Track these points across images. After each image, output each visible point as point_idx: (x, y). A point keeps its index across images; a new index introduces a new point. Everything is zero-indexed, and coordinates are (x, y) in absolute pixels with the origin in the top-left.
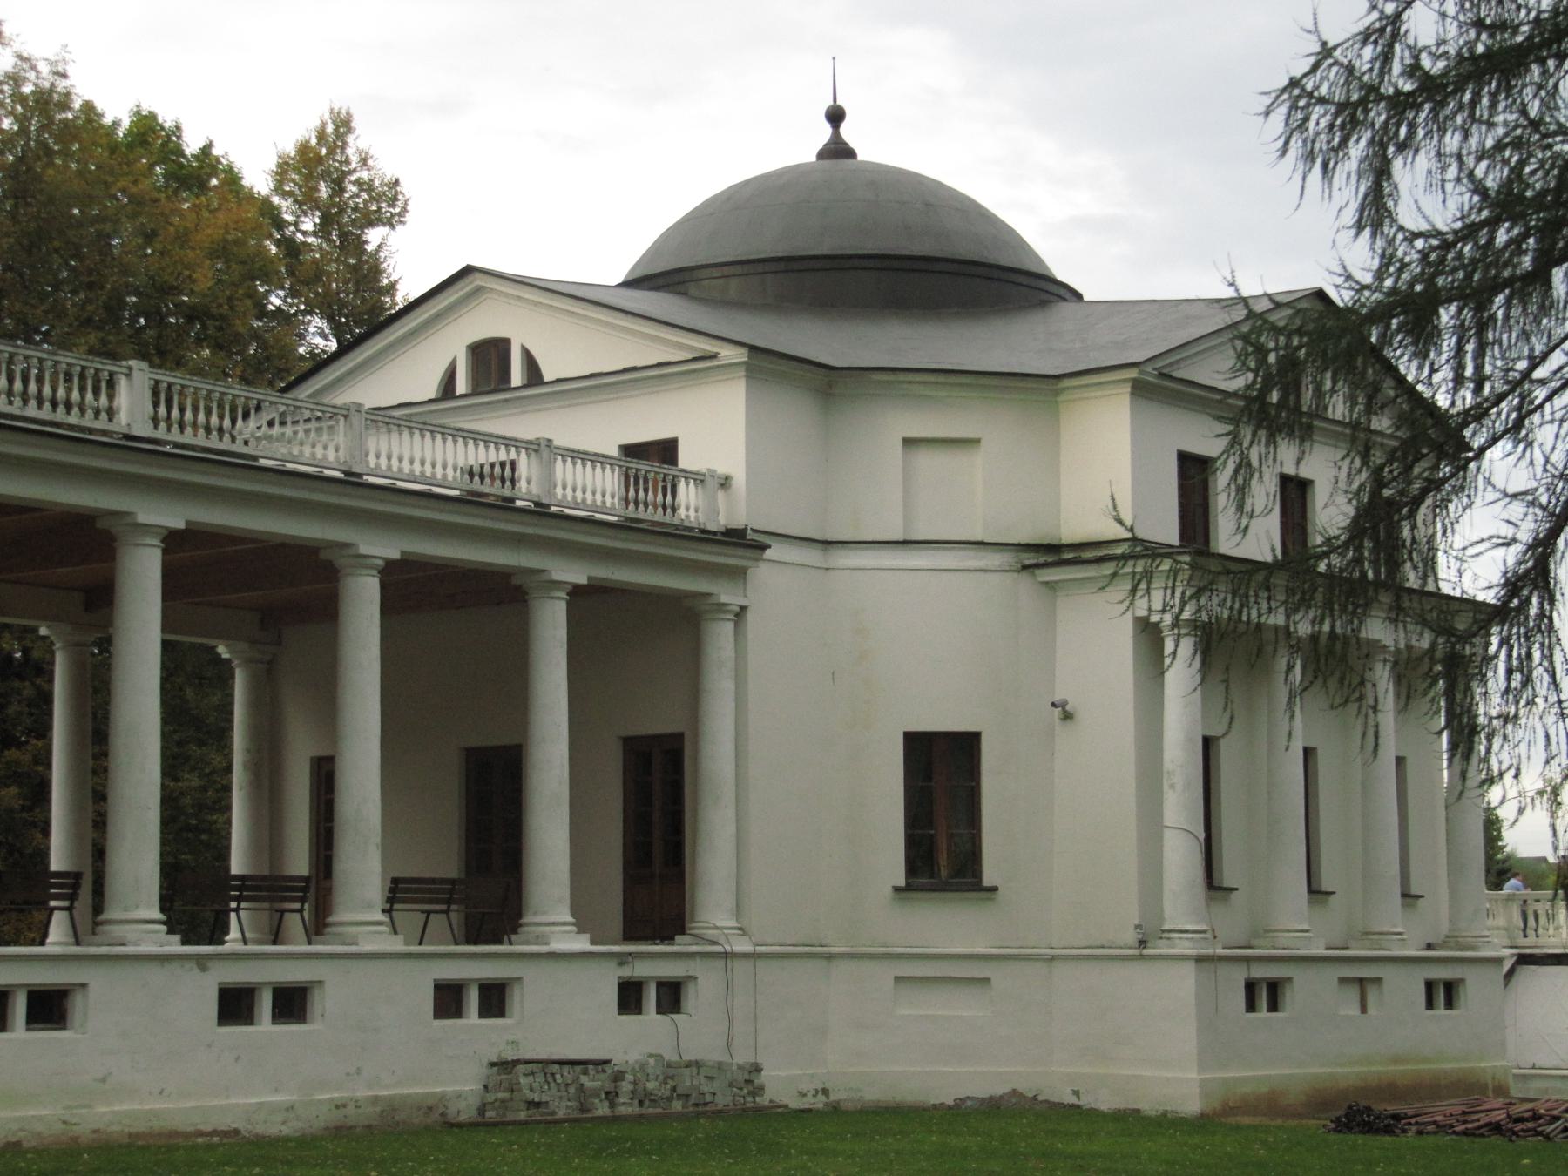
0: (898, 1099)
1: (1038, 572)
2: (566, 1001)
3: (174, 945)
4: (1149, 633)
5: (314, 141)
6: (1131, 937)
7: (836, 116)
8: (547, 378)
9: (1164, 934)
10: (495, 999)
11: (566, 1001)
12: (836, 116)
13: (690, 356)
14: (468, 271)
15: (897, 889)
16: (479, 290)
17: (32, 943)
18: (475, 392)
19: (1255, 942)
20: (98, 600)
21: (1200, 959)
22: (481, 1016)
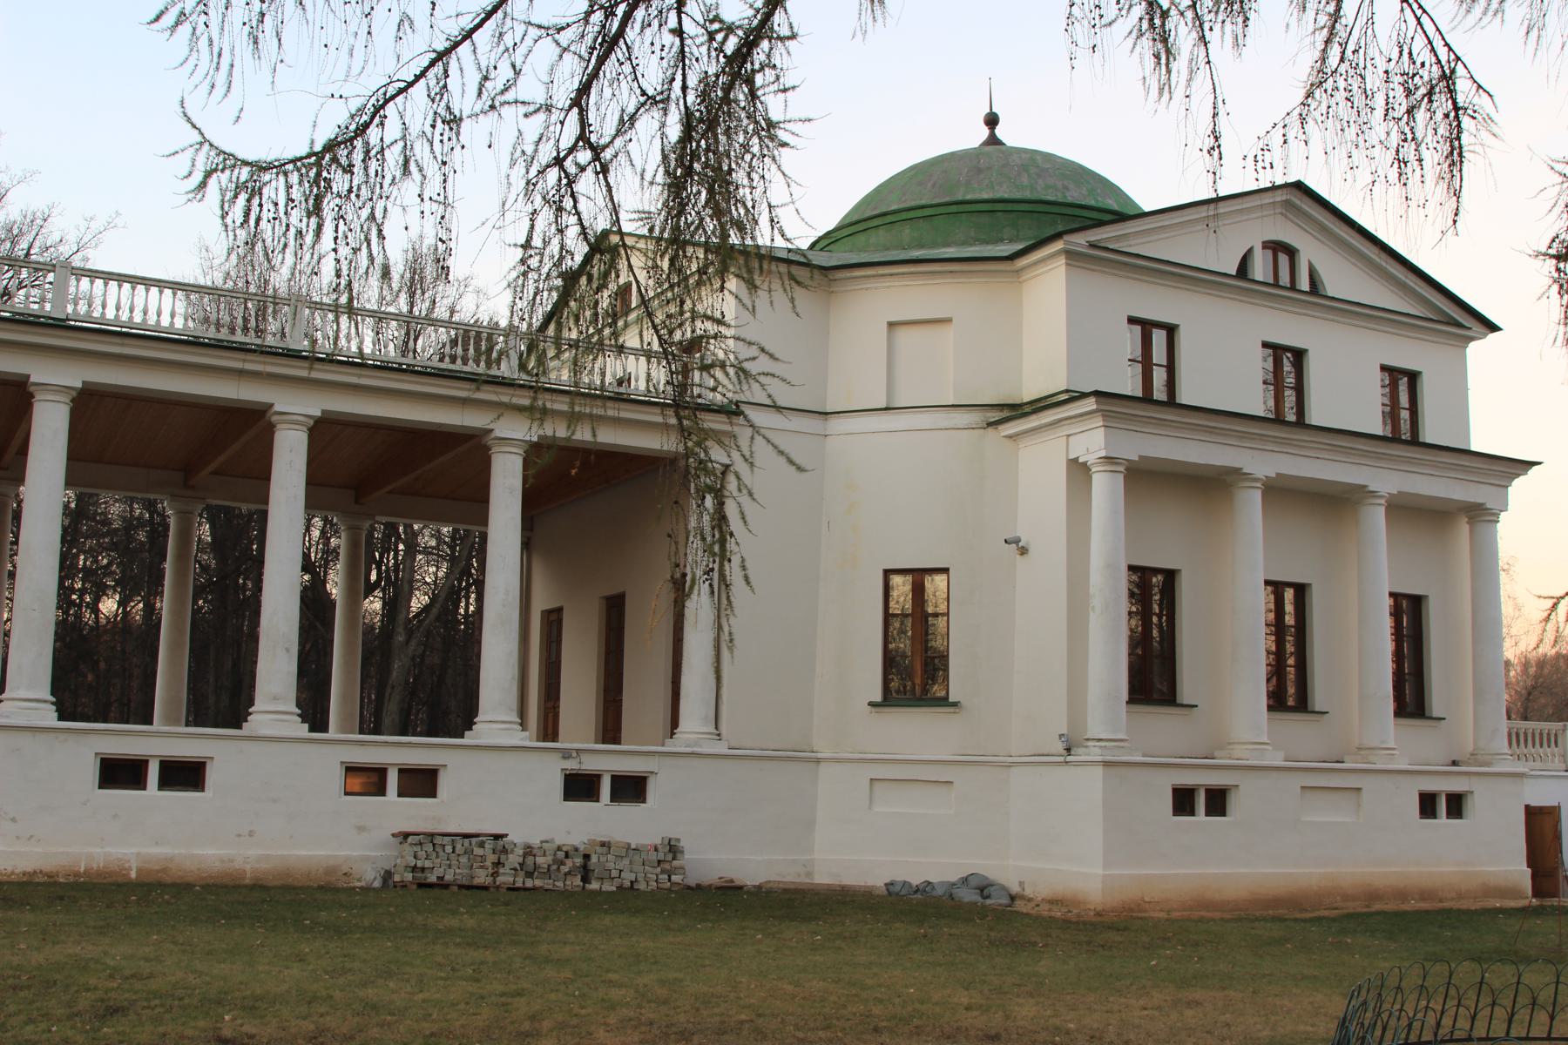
0: (870, 883)
1: (1001, 427)
2: (500, 787)
4: (1079, 470)
6: (1059, 747)
7: (992, 121)
10: (421, 782)
11: (500, 787)
12: (992, 121)
15: (872, 704)
19: (1216, 754)
20: (473, 500)
21: (1107, 764)
22: (1208, 814)
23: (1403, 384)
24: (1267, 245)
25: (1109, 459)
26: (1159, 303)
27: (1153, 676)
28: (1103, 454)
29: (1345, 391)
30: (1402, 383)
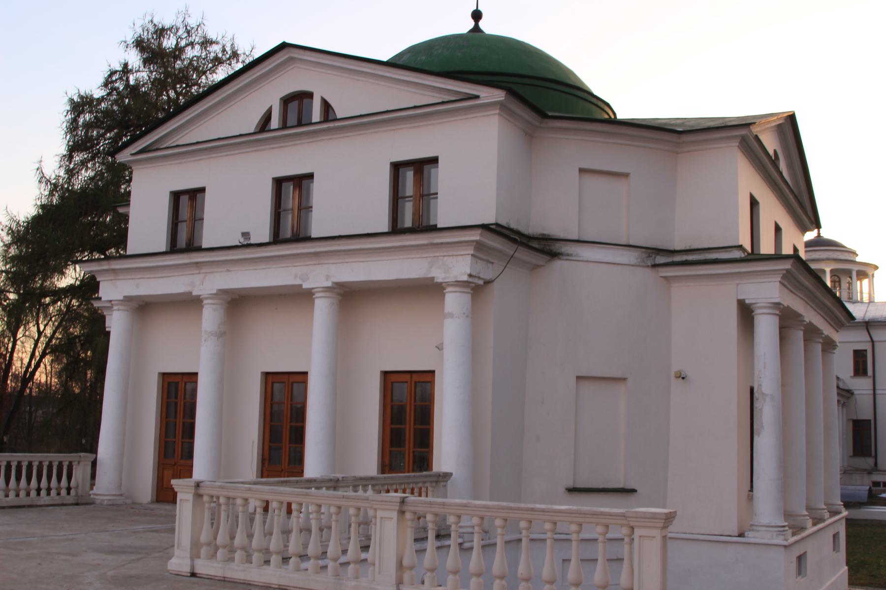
1: (660, 269)
5: (142, 75)
7: (477, 15)
8: (207, 242)
9: (752, 527)
12: (477, 15)
13: (440, 101)
14: (284, 46)
16: (291, 60)
17: (865, 356)
18: (284, 126)
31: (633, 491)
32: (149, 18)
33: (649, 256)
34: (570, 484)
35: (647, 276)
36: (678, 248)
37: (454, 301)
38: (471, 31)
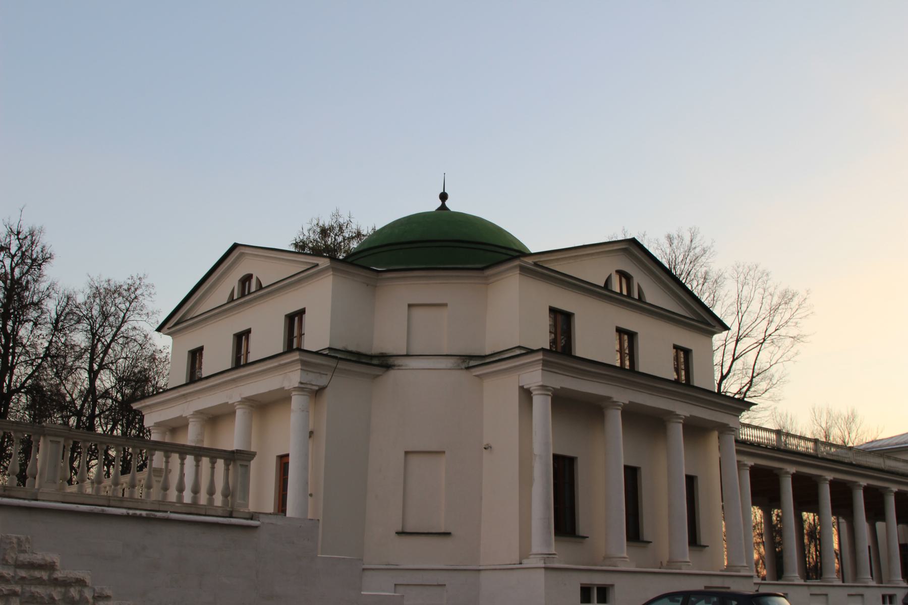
0: (869, 439)
3: (802, 582)
4: (526, 394)
7: (444, 197)
12: (444, 197)
14: (235, 246)
16: (242, 254)
21: (546, 568)
22: (598, 602)
23: (682, 354)
24: (618, 272)
25: (543, 387)
26: (566, 301)
27: (565, 522)
28: (541, 383)
29: (656, 358)
30: (684, 355)
31: (448, 534)
32: (315, 222)
33: (464, 362)
34: (400, 529)
35: (463, 375)
36: (487, 353)
37: (297, 400)
38: (439, 209)
